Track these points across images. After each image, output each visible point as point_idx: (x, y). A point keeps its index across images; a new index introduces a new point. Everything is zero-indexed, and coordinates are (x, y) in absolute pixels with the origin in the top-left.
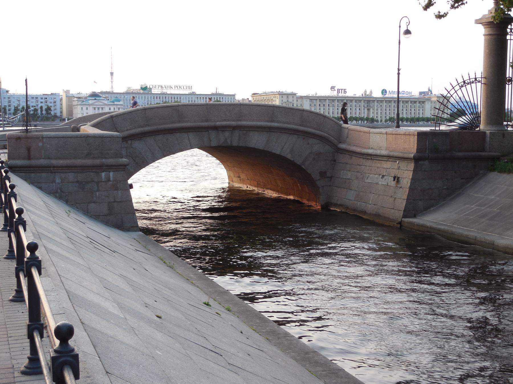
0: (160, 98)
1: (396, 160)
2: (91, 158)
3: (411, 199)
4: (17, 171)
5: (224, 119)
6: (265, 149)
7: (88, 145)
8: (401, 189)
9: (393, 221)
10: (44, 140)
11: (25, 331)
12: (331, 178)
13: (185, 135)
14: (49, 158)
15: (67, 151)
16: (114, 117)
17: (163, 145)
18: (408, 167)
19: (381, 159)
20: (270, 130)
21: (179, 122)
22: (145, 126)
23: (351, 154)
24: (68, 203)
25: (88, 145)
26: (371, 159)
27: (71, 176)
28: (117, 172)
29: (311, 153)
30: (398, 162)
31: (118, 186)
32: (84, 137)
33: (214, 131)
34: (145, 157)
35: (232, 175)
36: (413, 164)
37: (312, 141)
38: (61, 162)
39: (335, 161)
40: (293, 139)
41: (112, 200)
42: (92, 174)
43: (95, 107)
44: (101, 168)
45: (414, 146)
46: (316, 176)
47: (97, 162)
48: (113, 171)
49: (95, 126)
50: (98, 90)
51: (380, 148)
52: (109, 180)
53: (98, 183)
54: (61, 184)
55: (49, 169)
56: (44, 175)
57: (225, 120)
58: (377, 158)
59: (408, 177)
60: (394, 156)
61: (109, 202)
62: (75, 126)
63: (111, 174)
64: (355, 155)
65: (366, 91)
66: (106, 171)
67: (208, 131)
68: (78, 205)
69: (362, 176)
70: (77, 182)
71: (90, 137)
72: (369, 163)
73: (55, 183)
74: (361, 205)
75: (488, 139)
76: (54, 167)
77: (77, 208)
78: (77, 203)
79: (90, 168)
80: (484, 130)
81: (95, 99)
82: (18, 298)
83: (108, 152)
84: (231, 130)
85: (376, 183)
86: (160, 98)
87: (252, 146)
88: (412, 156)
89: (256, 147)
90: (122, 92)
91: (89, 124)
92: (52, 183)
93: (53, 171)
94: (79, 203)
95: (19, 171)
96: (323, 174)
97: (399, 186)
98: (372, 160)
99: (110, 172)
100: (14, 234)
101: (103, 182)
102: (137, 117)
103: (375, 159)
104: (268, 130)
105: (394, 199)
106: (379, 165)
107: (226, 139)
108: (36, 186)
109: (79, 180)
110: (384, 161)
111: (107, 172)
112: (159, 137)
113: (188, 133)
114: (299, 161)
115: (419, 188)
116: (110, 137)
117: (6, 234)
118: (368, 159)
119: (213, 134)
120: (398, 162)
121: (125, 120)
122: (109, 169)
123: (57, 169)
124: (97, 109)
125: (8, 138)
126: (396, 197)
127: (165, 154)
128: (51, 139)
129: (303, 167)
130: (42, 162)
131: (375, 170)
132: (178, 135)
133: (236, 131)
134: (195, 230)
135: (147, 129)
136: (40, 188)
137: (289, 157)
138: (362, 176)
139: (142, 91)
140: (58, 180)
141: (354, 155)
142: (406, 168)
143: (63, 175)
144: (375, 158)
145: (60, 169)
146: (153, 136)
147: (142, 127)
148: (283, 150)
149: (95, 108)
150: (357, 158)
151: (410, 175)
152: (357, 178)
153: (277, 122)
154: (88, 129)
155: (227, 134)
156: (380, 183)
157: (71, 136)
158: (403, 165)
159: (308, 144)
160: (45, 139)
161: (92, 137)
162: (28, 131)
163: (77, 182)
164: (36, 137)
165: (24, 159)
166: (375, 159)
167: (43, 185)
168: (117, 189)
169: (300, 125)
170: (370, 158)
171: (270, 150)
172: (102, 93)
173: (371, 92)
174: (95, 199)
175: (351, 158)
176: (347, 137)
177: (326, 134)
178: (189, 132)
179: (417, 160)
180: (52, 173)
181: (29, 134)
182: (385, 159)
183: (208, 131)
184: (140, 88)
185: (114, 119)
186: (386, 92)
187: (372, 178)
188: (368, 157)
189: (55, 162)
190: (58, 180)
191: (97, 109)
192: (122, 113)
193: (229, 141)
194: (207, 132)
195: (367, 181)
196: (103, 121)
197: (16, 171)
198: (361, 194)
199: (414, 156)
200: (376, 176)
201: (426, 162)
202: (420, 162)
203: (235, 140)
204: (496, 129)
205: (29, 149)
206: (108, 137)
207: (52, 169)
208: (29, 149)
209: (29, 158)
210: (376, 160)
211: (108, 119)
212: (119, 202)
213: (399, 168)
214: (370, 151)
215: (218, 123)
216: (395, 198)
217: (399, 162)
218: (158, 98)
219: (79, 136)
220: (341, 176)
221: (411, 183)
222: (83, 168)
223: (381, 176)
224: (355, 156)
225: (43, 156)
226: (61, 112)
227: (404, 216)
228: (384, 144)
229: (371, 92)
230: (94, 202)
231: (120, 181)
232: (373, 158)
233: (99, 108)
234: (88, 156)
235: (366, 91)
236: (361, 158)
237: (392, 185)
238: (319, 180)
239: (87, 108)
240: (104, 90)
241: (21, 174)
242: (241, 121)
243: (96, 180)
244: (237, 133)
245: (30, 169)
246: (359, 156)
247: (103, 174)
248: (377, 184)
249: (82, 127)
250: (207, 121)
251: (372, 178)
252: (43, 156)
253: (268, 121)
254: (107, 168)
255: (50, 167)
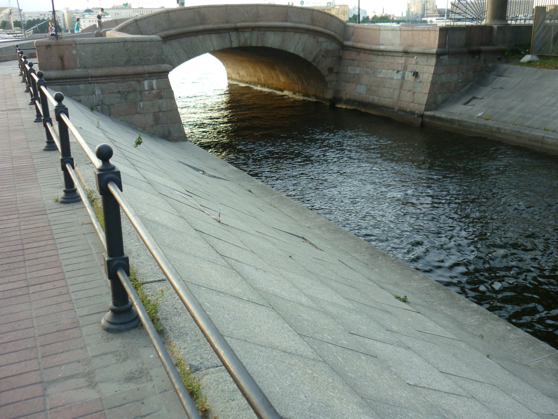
0: (138, 12)
1: (414, 56)
2: (131, 65)
3: (432, 93)
4: (51, 84)
5: (243, 20)
6: (281, 49)
7: (126, 51)
8: (421, 84)
9: (412, 113)
10: (78, 47)
11: (59, 165)
12: (337, 73)
13: (207, 37)
14: (85, 68)
15: (104, 59)
16: (138, 21)
17: (187, 47)
18: (429, 62)
19: (395, 55)
20: (284, 29)
21: (202, 24)
22: (169, 29)
23: (359, 51)
24: (111, 116)
25: (126, 51)
26: (383, 55)
27: (112, 86)
28: (160, 79)
29: (320, 51)
30: (416, 58)
31: (163, 94)
32: (121, 42)
33: (235, 33)
34: (171, 60)
35: (231, 72)
36: (434, 59)
37: (321, 39)
38: (99, 72)
39: (340, 57)
40: (305, 38)
41: (157, 110)
42: (133, 83)
43: (90, 20)
44: (140, 76)
45: (435, 41)
46: (324, 72)
47: (139, 69)
48: (156, 79)
49: (121, 30)
50: (90, 8)
51: (392, 44)
52: (151, 88)
53: (141, 93)
54: (101, 96)
55: (87, 79)
56: (82, 86)
57: (244, 21)
58: (389, 54)
59: (428, 71)
60: (413, 52)
61: (154, 112)
62: (98, 32)
63: (154, 82)
64: (363, 52)
65: (289, 3)
66: (148, 79)
67: (229, 32)
68: (121, 117)
69: (372, 71)
70: (119, 92)
71: (128, 41)
72: (380, 58)
73: (95, 94)
74: (374, 99)
75: (495, 33)
76: (92, 77)
77: (122, 121)
78: (120, 116)
79: (131, 76)
80: (490, 24)
81: (90, 14)
82: (51, 146)
83: (149, 58)
84: (251, 30)
85: (390, 78)
86: (138, 12)
87: (269, 45)
88: (434, 51)
89: (272, 47)
90: (110, 8)
91: (114, 29)
92: (92, 95)
93: (91, 82)
94: (123, 116)
95: (55, 84)
96: (330, 70)
97: (418, 80)
98: (384, 56)
99: (152, 80)
100: (49, 123)
101: (147, 91)
102: (161, 21)
103: (387, 55)
104: (283, 30)
105: (412, 93)
106: (392, 61)
107: (246, 40)
108: (75, 100)
109: (120, 90)
110: (399, 56)
111: (150, 80)
112: (184, 40)
113: (211, 35)
114: (310, 59)
115: (439, 82)
116: (150, 41)
117: (41, 124)
118: (378, 55)
119: (234, 35)
120: (416, 58)
121: (150, 23)
122: (151, 76)
123: (96, 79)
124: (91, 22)
125: (37, 46)
126: (414, 91)
127: (190, 56)
128: (85, 45)
129: (314, 64)
130: (78, 72)
131: (388, 65)
132: (201, 37)
133: (255, 32)
134: (269, 148)
135: (172, 32)
136: (79, 101)
137: (302, 55)
138: (372, 71)
139: (124, 7)
140: (98, 92)
141: (362, 51)
142: (425, 63)
143: (104, 86)
144: (387, 54)
145: (99, 79)
146: (178, 39)
147: (166, 30)
148: (296, 48)
149: (90, 21)
150: (366, 55)
151: (432, 70)
152: (367, 73)
153: (291, 22)
154: (112, 34)
155: (247, 35)
156: (395, 78)
157: (107, 42)
158: (422, 60)
159: (318, 42)
160: (79, 45)
161: (131, 41)
162: (58, 38)
163: (119, 92)
164: (68, 44)
165: (58, 69)
166: (387, 55)
167: (82, 98)
168: (161, 98)
169: (310, 25)
170: (381, 54)
171: (285, 49)
172: (94, 9)
173: (293, 3)
174: (139, 109)
175: (359, 54)
176: (352, 35)
177: (333, 33)
178: (212, 34)
179: (438, 55)
180: (90, 83)
181: (60, 41)
182: (400, 55)
183: (229, 32)
184: (122, 4)
185: (139, 22)
186: (303, 3)
187: (383, 73)
188: (378, 54)
189: (92, 72)
190: (98, 92)
191: (91, 22)
192: (146, 16)
193: (248, 41)
194: (228, 34)
195: (380, 76)
196: (127, 26)
197: (50, 84)
198: (373, 88)
199: (437, 52)
200: (390, 71)
201: (446, 57)
202: (441, 57)
203: (253, 40)
204: (500, 23)
205: (62, 58)
206: (147, 41)
207: (90, 79)
208: (62, 58)
209: (63, 68)
210: (389, 56)
211: (132, 23)
212: (164, 111)
213: (417, 63)
214: (382, 48)
215: (239, 25)
216: (414, 93)
217: (417, 58)
218: (137, 11)
219: (116, 41)
220: (349, 72)
221: (433, 77)
222: (124, 77)
223: (395, 71)
224: (363, 53)
225: (79, 66)
226: (65, 25)
227: (426, 110)
228: (397, 41)
229: (293, 3)
230: (139, 113)
231: (164, 89)
232: (384, 54)
233: (93, 21)
234: (128, 62)
235: (289, 3)
236: (370, 54)
237: (409, 80)
238: (327, 75)
239: (84, 21)
240: (96, 7)
241: (57, 86)
242: (258, 21)
243: (138, 90)
244: (255, 33)
245: (65, 81)
246: (367, 52)
247: (146, 83)
248: (392, 78)
249: (107, 32)
250: (227, 22)
251: (383, 73)
252: (79, 66)
253: (283, 21)
254: (149, 75)
255: (87, 77)
